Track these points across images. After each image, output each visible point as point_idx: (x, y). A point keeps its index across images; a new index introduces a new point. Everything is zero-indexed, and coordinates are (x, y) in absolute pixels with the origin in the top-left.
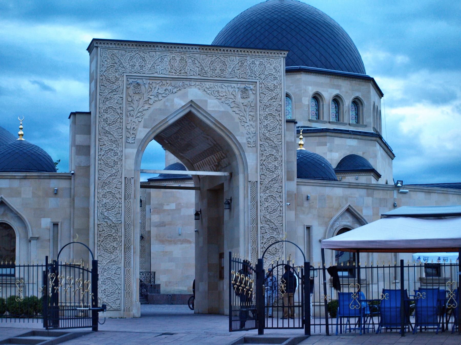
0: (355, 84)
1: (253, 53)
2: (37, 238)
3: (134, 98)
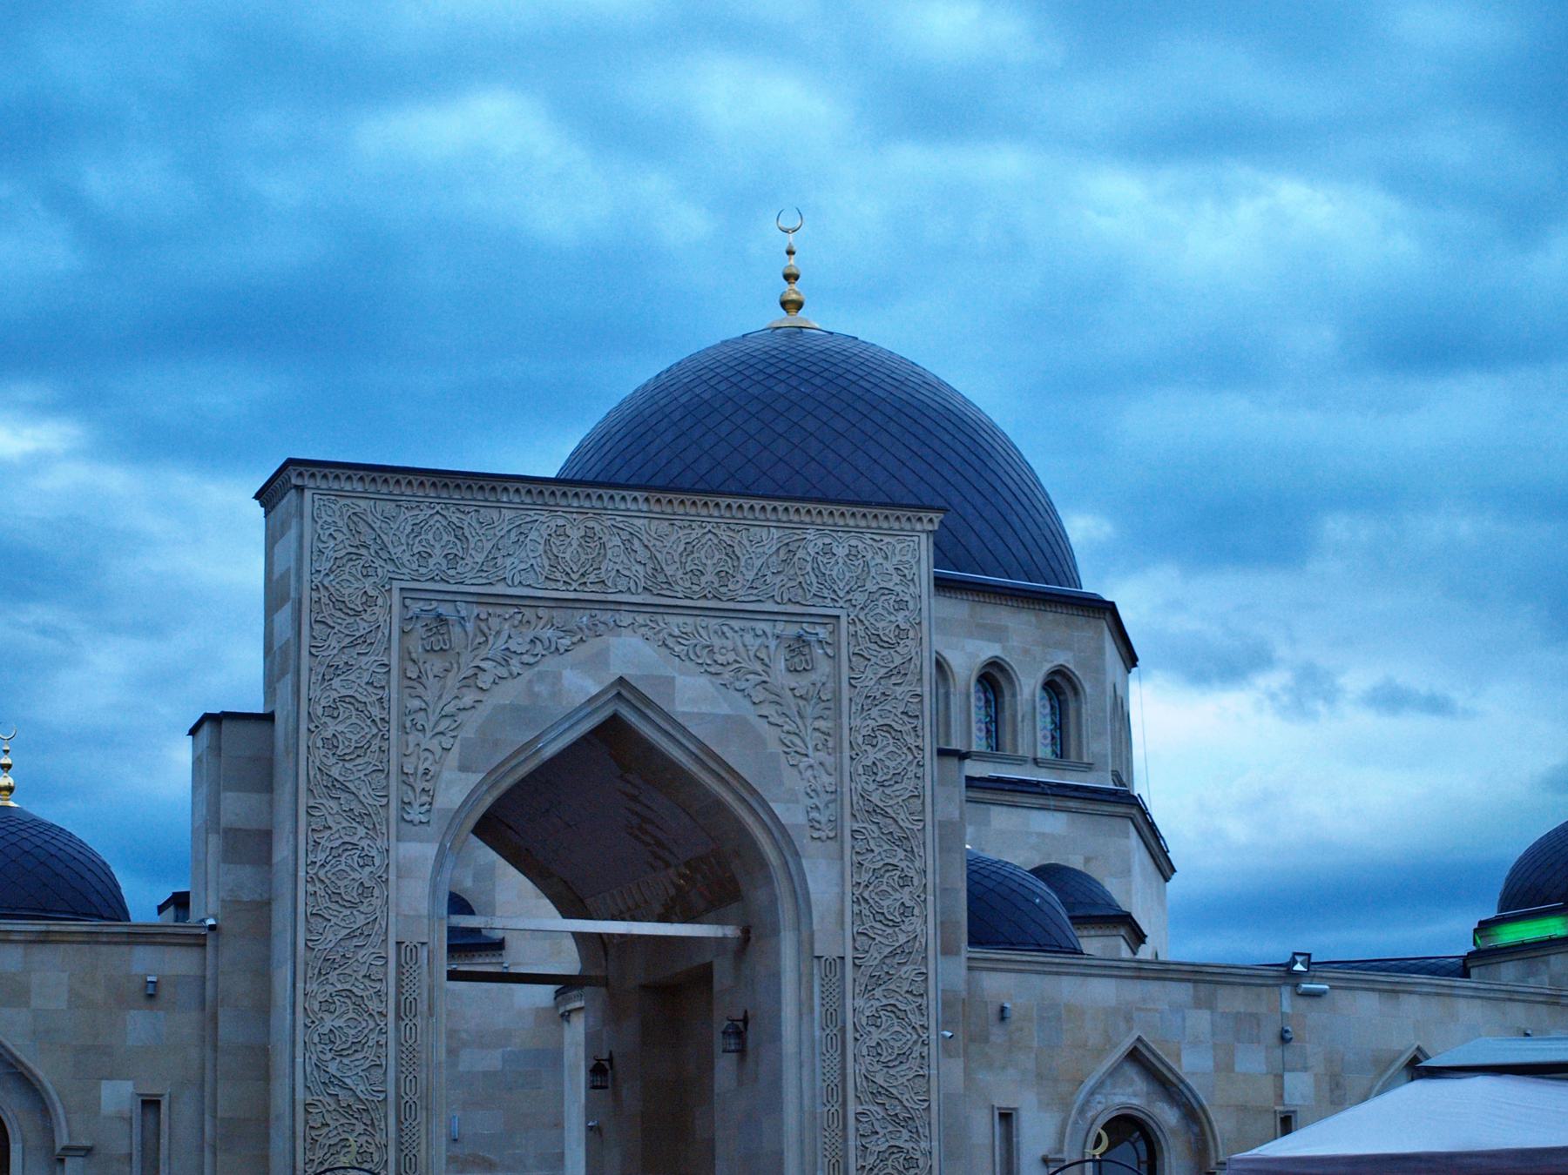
0: (1054, 623)
1: (826, 518)
2: (88, 1151)
3: (428, 666)
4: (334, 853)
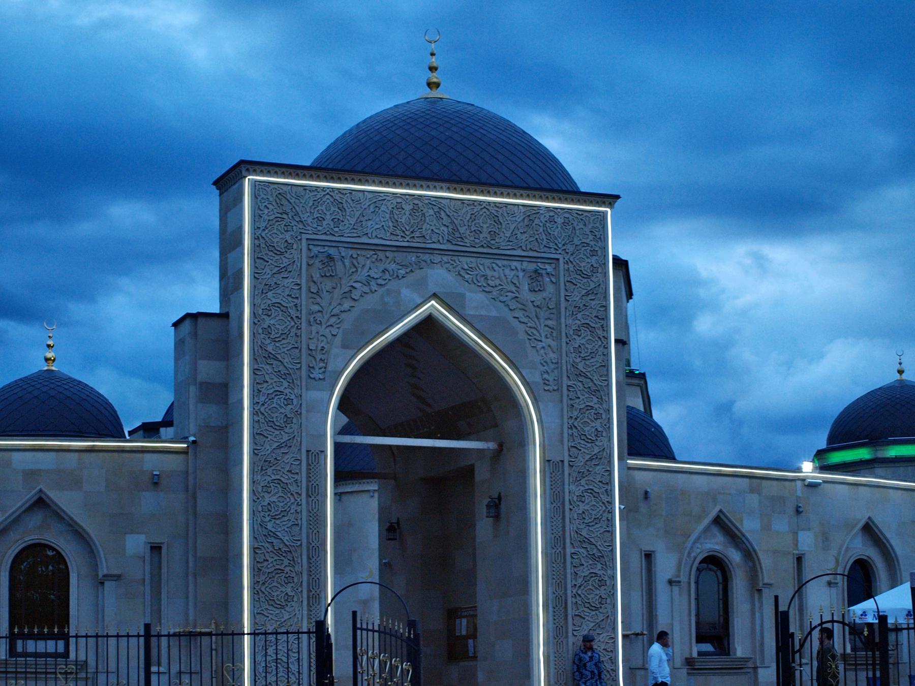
2: (118, 577)
4: (270, 397)
